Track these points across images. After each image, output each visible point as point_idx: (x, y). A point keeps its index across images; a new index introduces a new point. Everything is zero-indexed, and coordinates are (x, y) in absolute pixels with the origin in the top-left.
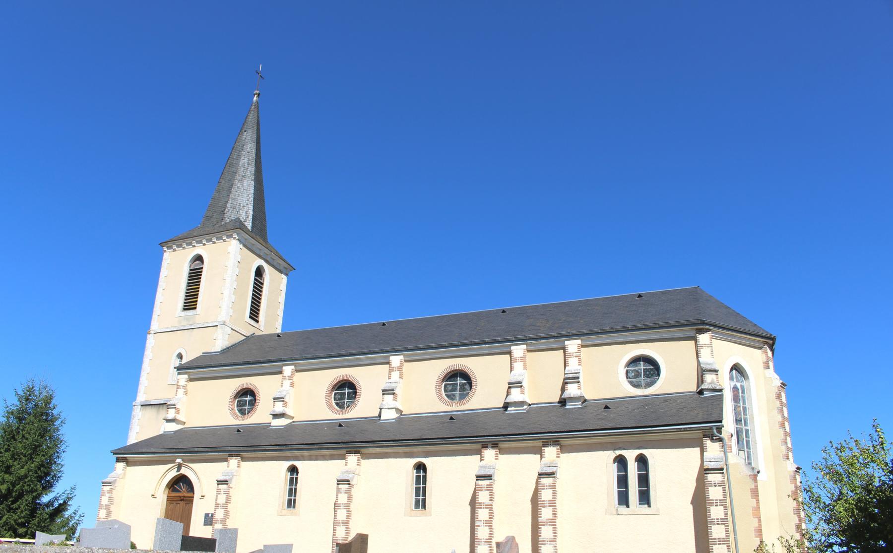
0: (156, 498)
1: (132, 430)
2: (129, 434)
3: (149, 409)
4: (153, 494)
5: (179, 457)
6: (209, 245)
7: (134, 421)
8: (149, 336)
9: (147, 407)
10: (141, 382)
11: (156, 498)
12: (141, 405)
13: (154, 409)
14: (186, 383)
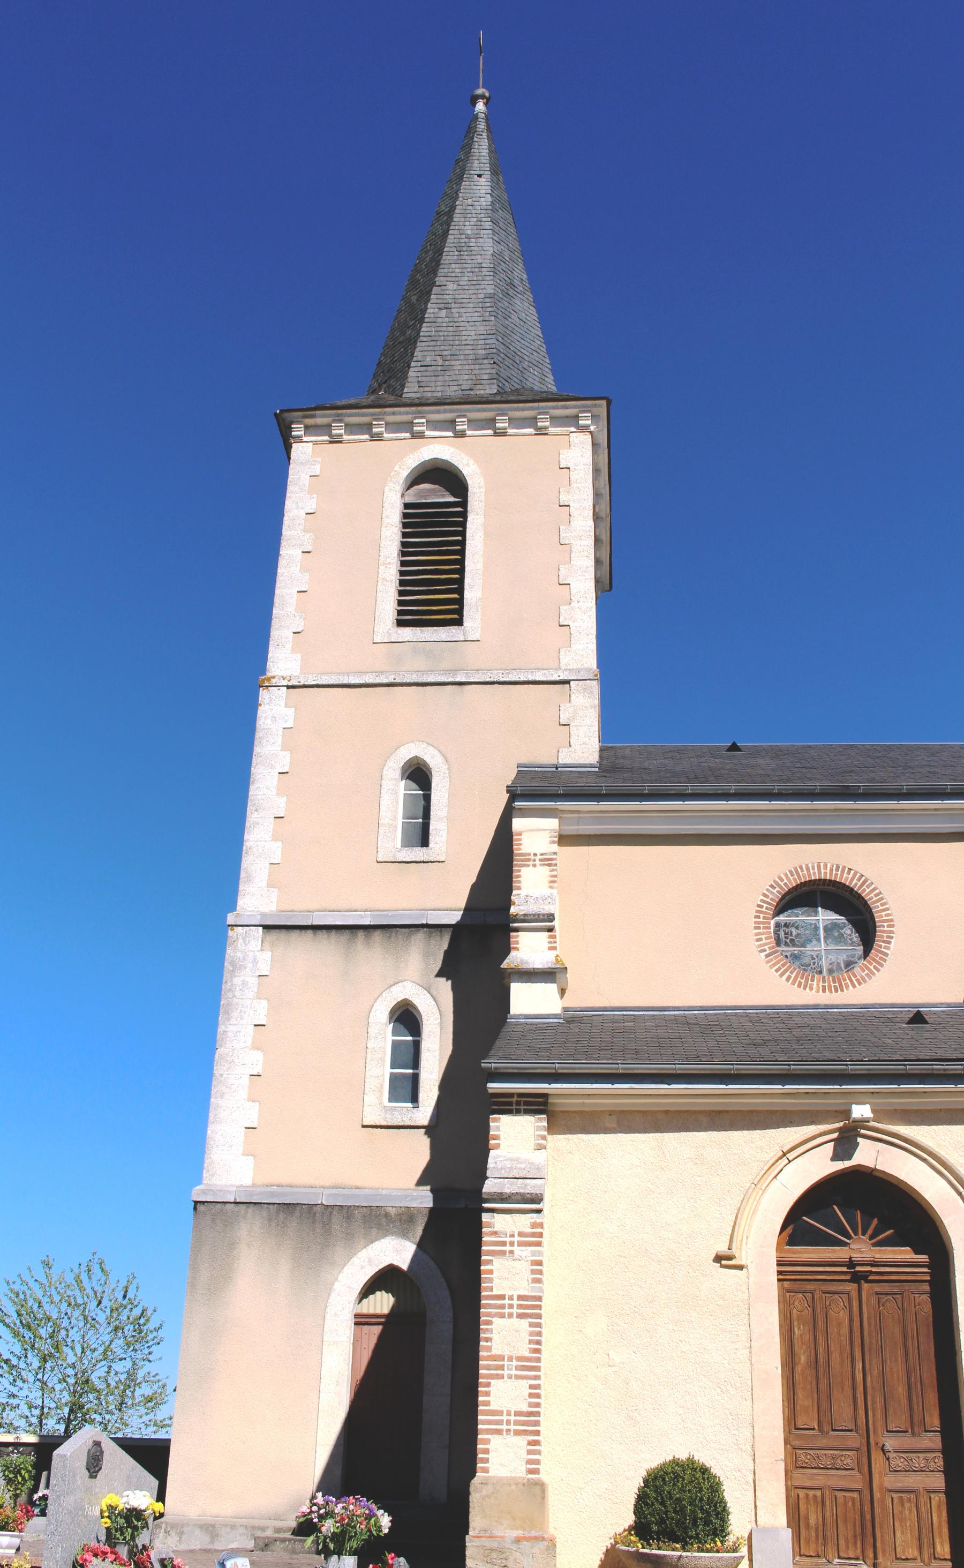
0: (740, 1267)
1: (235, 1014)
2: (221, 1028)
3: (302, 944)
4: (723, 1248)
5: (861, 1098)
6: (481, 440)
7: (237, 981)
8: (264, 695)
9: (295, 934)
10: (247, 845)
11: (740, 1267)
12: (266, 927)
13: (329, 946)
14: (555, 847)
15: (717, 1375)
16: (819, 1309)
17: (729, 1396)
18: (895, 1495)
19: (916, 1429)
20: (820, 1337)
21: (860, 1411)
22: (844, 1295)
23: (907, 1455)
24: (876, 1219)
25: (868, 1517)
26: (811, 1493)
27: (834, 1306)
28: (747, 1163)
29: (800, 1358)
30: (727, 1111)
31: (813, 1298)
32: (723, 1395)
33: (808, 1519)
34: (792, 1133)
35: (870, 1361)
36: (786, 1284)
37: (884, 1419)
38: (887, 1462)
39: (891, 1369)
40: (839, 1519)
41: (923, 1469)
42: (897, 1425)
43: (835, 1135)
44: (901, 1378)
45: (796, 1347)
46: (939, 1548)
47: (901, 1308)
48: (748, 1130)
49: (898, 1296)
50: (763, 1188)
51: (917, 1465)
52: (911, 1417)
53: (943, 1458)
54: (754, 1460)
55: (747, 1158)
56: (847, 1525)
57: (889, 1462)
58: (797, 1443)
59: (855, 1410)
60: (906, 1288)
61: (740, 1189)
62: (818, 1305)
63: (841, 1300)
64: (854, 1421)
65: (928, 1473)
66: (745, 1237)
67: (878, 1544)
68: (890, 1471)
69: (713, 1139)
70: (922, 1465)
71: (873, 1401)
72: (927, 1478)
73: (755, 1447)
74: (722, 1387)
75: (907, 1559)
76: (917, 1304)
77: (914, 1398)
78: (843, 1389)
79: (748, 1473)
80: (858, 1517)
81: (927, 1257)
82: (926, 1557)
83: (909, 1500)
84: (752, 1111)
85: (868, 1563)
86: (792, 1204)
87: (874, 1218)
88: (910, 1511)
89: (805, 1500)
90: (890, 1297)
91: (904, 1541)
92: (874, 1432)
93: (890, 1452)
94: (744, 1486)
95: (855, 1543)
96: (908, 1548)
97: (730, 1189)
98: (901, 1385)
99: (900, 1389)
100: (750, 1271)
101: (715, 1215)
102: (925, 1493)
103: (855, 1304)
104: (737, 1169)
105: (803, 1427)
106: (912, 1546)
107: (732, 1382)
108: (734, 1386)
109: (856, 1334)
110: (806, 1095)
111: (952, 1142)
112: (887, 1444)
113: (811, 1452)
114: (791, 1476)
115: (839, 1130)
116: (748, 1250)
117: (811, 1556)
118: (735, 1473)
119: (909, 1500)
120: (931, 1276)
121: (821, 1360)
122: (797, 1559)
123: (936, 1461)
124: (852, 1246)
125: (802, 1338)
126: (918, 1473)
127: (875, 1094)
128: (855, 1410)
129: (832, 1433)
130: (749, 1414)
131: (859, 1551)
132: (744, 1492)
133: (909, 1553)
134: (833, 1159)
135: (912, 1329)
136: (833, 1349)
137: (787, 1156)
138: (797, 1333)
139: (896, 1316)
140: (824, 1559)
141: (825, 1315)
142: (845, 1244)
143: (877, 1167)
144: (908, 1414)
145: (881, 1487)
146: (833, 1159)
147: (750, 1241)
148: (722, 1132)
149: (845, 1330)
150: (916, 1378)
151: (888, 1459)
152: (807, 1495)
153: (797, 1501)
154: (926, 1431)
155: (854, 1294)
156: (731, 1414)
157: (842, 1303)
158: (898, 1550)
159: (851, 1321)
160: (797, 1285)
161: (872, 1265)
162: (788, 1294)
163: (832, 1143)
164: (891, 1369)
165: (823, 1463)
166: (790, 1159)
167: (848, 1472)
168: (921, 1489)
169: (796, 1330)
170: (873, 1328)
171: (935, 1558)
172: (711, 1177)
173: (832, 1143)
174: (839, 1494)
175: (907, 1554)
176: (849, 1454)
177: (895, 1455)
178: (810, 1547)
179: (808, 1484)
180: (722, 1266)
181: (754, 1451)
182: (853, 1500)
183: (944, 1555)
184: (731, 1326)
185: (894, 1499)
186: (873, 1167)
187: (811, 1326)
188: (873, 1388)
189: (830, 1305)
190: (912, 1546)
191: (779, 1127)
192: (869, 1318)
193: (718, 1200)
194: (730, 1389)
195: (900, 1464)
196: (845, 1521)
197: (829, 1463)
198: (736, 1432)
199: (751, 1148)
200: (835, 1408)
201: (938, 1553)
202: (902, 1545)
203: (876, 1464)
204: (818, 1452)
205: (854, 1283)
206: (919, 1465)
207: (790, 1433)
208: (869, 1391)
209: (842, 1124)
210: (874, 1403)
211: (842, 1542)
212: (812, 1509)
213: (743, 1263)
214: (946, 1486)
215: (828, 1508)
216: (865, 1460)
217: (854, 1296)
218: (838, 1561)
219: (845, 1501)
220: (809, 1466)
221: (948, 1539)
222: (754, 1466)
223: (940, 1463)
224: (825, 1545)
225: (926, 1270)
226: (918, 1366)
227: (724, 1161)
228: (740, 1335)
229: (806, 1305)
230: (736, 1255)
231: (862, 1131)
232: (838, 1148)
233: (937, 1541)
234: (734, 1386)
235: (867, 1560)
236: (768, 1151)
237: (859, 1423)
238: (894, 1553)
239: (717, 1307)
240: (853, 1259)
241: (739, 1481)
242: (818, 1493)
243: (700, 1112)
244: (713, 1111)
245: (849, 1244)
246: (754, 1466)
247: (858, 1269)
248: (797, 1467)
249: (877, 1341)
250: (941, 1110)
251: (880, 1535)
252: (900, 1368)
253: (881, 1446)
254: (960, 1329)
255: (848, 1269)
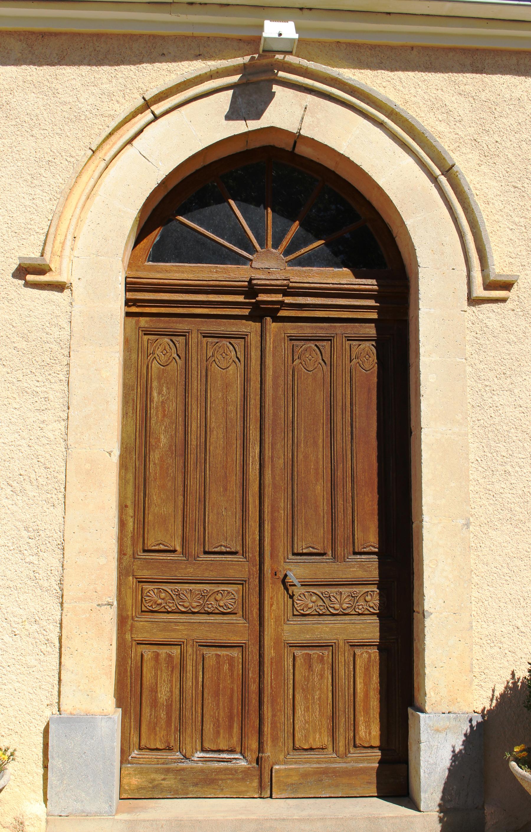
0: (59, 287)
11: (59, 287)
15: (7, 464)
16: (195, 361)
17: (25, 499)
18: (299, 653)
19: (339, 549)
20: (194, 406)
21: (252, 523)
22: (238, 341)
23: (323, 590)
24: (297, 222)
25: (254, 687)
26: (163, 651)
27: (220, 357)
28: (83, 117)
29: (158, 440)
30: (56, 35)
31: (187, 344)
32: (15, 497)
33: (157, 692)
34: (164, 73)
35: (273, 445)
36: (143, 321)
37: (290, 535)
38: (290, 601)
39: (306, 457)
40: (206, 691)
41: (346, 612)
42: (308, 545)
43: (235, 78)
44: (320, 471)
45: (153, 422)
46: (362, 731)
47: (328, 362)
48: (89, 65)
49: (325, 343)
50: (108, 158)
51: (337, 606)
52: (333, 531)
53: (380, 595)
54: (62, 604)
55: (84, 109)
56: (218, 700)
57: (293, 601)
58: (145, 574)
59: (244, 520)
60: (339, 332)
61: (69, 159)
62: (194, 355)
63: (231, 348)
64: (240, 537)
65: (353, 617)
66: (70, 237)
67: (267, 729)
68: (294, 615)
69: (29, 78)
70: (345, 606)
71: (273, 507)
72: (351, 626)
73: (65, 583)
74: (15, 484)
75: (311, 749)
76: (353, 356)
77: (340, 502)
78: (226, 489)
79: (51, 627)
80: (237, 687)
81: (374, 282)
82: (341, 744)
83: (321, 659)
84: (98, 36)
85: (249, 758)
86: (154, 185)
87: (295, 221)
88: (322, 676)
89: (153, 663)
90: (312, 345)
91: (307, 722)
92: (272, 556)
93: (295, 585)
94: (43, 647)
95: (231, 727)
96: (314, 732)
97: (50, 159)
98: (321, 481)
99: (319, 488)
100: (74, 292)
101: (23, 200)
102: (347, 647)
103: (255, 354)
104: (66, 128)
105: (157, 548)
106: (320, 729)
107: (33, 476)
108: (35, 483)
109: (253, 402)
110: (190, 7)
111: (426, 97)
112: (290, 574)
113: (168, 587)
114: (132, 626)
115: (243, 69)
116: (75, 260)
117: (157, 749)
118: (28, 626)
119: (321, 659)
120: (378, 313)
121: (193, 442)
122: (133, 755)
123: (368, 598)
124: (255, 265)
125: (163, 408)
126: (339, 618)
127: (306, 12)
128: (244, 520)
129: (203, 557)
130: (57, 529)
131: (235, 740)
132: (42, 657)
133: (314, 740)
134: (229, 117)
135: (344, 396)
136: (213, 425)
137: (153, 108)
138: (156, 399)
139: (320, 375)
140: (178, 754)
141: (204, 373)
142: (244, 261)
143: (302, 132)
144: (327, 526)
145: (278, 641)
146: (229, 117)
147: (79, 243)
148: (45, 67)
149: (236, 395)
150: (344, 471)
151: (291, 597)
152: (157, 655)
153: (139, 664)
154: (355, 553)
155: (254, 339)
156: (26, 529)
157: (233, 353)
158: (298, 735)
159: (246, 380)
160: (161, 324)
161: (286, 294)
162: (146, 338)
163: (230, 92)
164: (306, 457)
165: (187, 604)
166: (157, 112)
167: (226, 617)
168: (341, 643)
169: (155, 394)
170: (280, 392)
171: (355, 746)
172: (20, 139)
173: (230, 92)
174: (210, 653)
175: (311, 740)
176: (229, 589)
177: (303, 590)
178: (156, 735)
179: (159, 637)
180: (28, 284)
181: (62, 590)
182: (231, 660)
183: (369, 741)
184: (38, 384)
185: (298, 659)
186: (295, 132)
187: (181, 389)
188: (275, 486)
189: (213, 356)
190: (320, 729)
191: (141, 62)
192: (275, 378)
193: (29, 177)
194: (28, 487)
195: (311, 605)
196: (216, 694)
197: (195, 606)
198: (34, 559)
199: (93, 94)
200: (211, 517)
201: (360, 739)
202: (304, 729)
203: (271, 605)
204: (178, 587)
205: (254, 321)
206: (341, 605)
207: (134, 558)
208: (268, 490)
209: (247, 59)
210: (274, 509)
211: (209, 727)
212: (164, 676)
213: (63, 278)
214: (381, 638)
215: (189, 675)
216: (255, 599)
217: (253, 342)
218: (202, 755)
219: (218, 663)
220: (163, 610)
221: (378, 716)
222: (61, 615)
223: (374, 601)
224: (180, 730)
225: (371, 303)
226: (349, 452)
227: (45, 115)
228: (51, 397)
229: (175, 356)
230: (52, 266)
231: (281, 74)
232: (240, 100)
233: (361, 719)
234: (35, 483)
235: (248, 754)
236: (122, 100)
237: (248, 540)
238: (291, 741)
239: (14, 352)
240: (254, 282)
241: (35, 638)
242: (176, 651)
243: (10, 33)
244: (33, 33)
245: (251, 260)
246: (61, 615)
247: (262, 297)
248: (142, 611)
249: (286, 413)
250: (412, 48)
251: (270, 714)
252: (320, 456)
253: (282, 577)
254: (422, 392)
255: (245, 298)
